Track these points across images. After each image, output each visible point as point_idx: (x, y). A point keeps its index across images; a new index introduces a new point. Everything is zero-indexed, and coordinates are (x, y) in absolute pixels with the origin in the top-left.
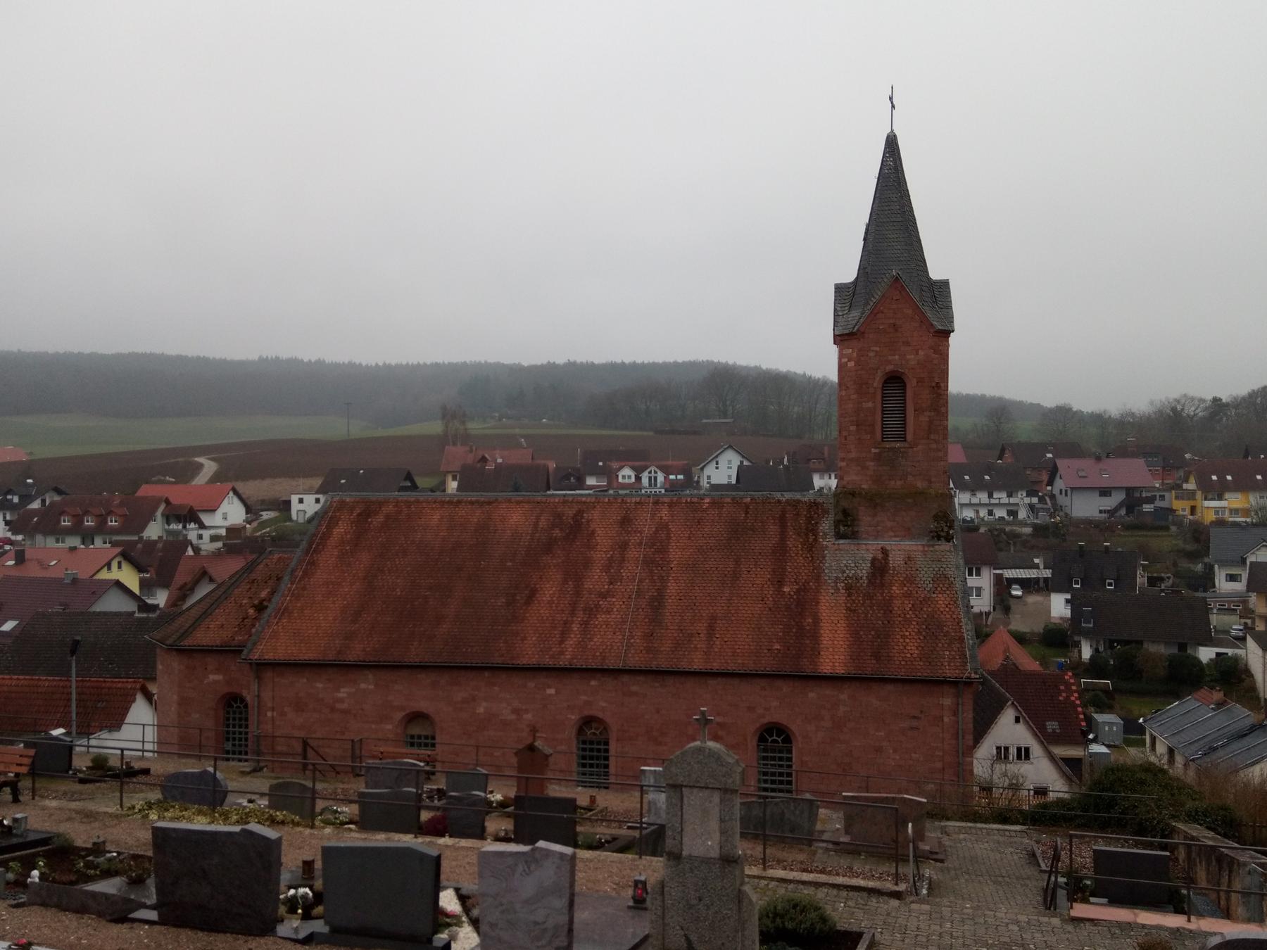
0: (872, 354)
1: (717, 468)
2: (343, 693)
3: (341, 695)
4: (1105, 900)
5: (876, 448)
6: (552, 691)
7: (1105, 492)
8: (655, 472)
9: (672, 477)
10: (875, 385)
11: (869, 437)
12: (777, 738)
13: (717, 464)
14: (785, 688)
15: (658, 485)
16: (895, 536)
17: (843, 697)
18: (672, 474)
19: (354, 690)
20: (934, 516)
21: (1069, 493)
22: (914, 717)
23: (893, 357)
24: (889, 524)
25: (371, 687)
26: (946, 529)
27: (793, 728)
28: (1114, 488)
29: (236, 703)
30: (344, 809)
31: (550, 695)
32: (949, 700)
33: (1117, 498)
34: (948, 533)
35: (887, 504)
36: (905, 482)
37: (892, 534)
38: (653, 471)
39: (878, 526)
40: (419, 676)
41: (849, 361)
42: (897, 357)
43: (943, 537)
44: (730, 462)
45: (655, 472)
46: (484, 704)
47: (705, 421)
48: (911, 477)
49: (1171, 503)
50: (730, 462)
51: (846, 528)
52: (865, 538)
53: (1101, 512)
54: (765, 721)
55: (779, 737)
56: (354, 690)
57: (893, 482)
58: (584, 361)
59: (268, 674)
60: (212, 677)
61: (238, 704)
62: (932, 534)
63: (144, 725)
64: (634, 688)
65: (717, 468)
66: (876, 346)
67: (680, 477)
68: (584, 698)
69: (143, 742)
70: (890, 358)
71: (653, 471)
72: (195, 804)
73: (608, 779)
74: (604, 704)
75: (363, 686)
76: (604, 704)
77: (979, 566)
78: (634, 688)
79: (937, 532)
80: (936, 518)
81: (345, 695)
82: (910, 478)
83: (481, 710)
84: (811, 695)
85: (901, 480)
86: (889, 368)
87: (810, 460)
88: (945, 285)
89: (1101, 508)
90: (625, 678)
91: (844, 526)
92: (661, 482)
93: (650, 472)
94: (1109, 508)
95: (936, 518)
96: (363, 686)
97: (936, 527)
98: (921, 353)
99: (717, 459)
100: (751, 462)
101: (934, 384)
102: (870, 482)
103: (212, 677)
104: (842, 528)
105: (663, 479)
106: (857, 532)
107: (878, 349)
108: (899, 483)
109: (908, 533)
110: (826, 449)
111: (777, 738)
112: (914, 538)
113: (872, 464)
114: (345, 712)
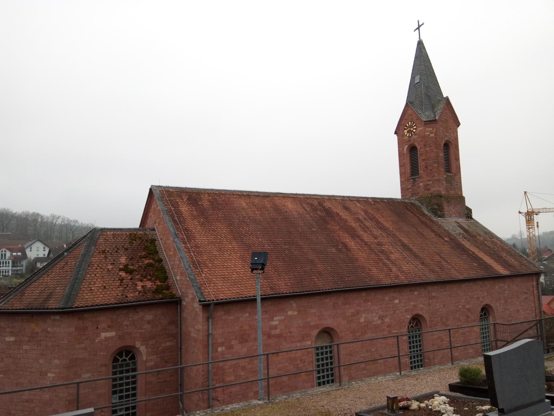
1: (31, 251)
2: (277, 320)
3: (274, 323)
6: (397, 301)
8: (5, 251)
9: (14, 254)
13: (31, 248)
14: (488, 284)
15: (7, 258)
16: (456, 216)
18: (15, 252)
19: (283, 317)
24: (454, 211)
25: (295, 313)
29: (126, 356)
31: (396, 304)
38: (4, 251)
40: (325, 300)
44: (38, 247)
45: (5, 251)
46: (364, 315)
50: (38, 247)
56: (283, 317)
59: (220, 313)
60: (103, 335)
61: (124, 358)
63: (397, 337)
64: (434, 294)
65: (31, 251)
67: (19, 254)
68: (412, 303)
69: (268, 379)
71: (4, 251)
73: (135, 400)
74: (422, 306)
75: (290, 313)
76: (422, 306)
78: (434, 294)
81: (277, 323)
83: (362, 320)
90: (430, 288)
92: (9, 257)
93: (2, 251)
96: (290, 313)
99: (31, 246)
102: (445, 191)
103: (103, 335)
105: (10, 255)
114: (279, 336)
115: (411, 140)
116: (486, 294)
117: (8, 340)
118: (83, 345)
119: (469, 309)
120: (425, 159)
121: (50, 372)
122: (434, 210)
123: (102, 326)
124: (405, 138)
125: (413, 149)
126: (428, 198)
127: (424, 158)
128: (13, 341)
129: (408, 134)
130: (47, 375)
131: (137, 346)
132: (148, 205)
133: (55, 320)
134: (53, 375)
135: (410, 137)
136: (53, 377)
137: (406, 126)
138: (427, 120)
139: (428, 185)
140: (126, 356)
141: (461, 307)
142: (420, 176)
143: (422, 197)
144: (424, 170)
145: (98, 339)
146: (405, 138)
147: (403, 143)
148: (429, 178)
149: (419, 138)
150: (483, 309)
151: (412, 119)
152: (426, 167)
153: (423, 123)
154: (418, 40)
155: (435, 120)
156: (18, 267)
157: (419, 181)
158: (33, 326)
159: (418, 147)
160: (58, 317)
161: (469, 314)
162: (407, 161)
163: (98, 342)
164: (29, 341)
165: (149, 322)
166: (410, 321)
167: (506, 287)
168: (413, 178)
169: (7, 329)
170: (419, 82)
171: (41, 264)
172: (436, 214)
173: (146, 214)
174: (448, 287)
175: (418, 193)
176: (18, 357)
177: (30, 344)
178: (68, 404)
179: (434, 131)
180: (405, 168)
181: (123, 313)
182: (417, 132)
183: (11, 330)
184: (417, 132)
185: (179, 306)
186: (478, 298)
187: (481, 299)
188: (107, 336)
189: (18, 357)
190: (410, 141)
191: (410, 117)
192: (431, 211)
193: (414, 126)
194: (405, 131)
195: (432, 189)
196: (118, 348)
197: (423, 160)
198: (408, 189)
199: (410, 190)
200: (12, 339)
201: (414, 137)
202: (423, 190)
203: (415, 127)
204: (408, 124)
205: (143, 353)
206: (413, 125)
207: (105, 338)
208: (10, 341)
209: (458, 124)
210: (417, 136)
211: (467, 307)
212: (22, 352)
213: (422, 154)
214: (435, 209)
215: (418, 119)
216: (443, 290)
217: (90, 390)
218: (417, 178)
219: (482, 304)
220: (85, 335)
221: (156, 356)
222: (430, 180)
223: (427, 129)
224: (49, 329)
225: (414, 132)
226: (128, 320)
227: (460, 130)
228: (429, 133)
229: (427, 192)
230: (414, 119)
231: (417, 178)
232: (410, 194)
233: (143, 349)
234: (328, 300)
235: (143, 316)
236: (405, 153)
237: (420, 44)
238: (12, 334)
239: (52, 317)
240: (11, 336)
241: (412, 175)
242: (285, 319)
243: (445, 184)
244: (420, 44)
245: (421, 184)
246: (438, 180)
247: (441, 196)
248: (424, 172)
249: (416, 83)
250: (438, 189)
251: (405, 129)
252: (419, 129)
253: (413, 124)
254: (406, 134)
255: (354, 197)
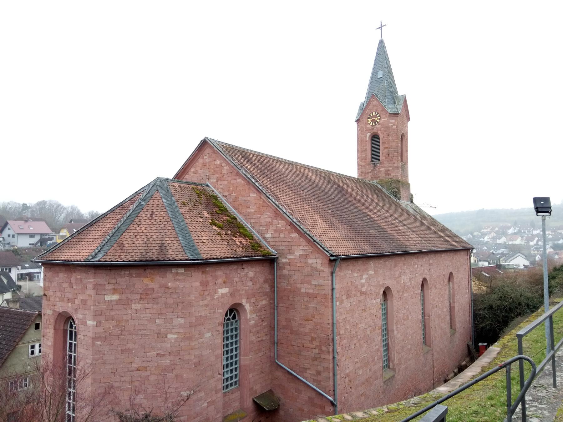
4: (525, 257)
7: (32, 236)
21: (16, 236)
28: (36, 234)
33: (37, 238)
41: (393, 125)
49: (56, 240)
53: (30, 244)
72: (529, 317)
77: (10, 267)
89: (30, 243)
94: (33, 243)
115: (375, 129)
117: (109, 299)
118: (205, 302)
120: (388, 147)
121: (171, 333)
122: (395, 193)
123: (220, 281)
124: (368, 126)
125: (375, 137)
126: (389, 182)
127: (387, 146)
128: (116, 300)
129: (372, 123)
130: (167, 337)
131: (244, 304)
132: (192, 160)
133: (177, 274)
134: (176, 336)
135: (374, 126)
136: (175, 339)
137: (370, 115)
138: (392, 112)
139: (389, 170)
140: (230, 316)
142: (381, 161)
143: (383, 181)
144: (385, 157)
145: (217, 295)
146: (368, 126)
147: (366, 131)
148: (390, 165)
149: (382, 128)
150: (231, 310)
151: (377, 110)
152: (388, 155)
153: (389, 115)
154: (380, 38)
155: (398, 114)
157: (380, 166)
158: (146, 281)
159: (381, 136)
160: (182, 270)
162: (369, 147)
163: (216, 298)
164: (141, 299)
165: (251, 280)
166: (227, 312)
168: (374, 164)
169: (107, 285)
170: (382, 77)
172: (396, 196)
173: (186, 168)
174: (438, 255)
175: (379, 177)
176: (124, 319)
177: (142, 302)
178: (194, 367)
179: (396, 123)
180: (366, 154)
181: (234, 268)
182: (381, 122)
183: (113, 287)
184: (381, 122)
185: (275, 263)
188: (223, 292)
189: (124, 319)
190: (373, 129)
191: (375, 108)
192: (392, 194)
193: (379, 116)
194: (368, 120)
195: (392, 175)
196: (231, 305)
197: (386, 148)
198: (368, 173)
199: (371, 174)
200: (115, 297)
201: (378, 126)
202: (384, 175)
203: (379, 118)
204: (372, 114)
205: (247, 310)
206: (378, 116)
207: (221, 294)
208: (111, 301)
209: (409, 119)
210: (381, 126)
212: (130, 313)
213: (385, 142)
214: (396, 192)
215: (384, 110)
217: (210, 351)
218: (379, 163)
220: (207, 290)
221: (256, 314)
222: (391, 167)
223: (391, 121)
224: (169, 284)
225: (378, 122)
226: (237, 277)
227: (409, 124)
228: (392, 125)
229: (388, 176)
230: (378, 110)
231: (379, 163)
232: (370, 177)
233: (247, 307)
234: (387, 262)
235: (247, 273)
236: (367, 139)
237: (381, 42)
238: (115, 291)
239: (174, 270)
240: (113, 294)
241: (372, 161)
242: (368, 278)
243: (401, 171)
244: (381, 42)
245: (382, 169)
246: (397, 167)
247: (399, 181)
248: (385, 159)
249: (379, 77)
250: (397, 175)
251: (369, 118)
252: (382, 120)
253: (377, 115)
254: (369, 122)
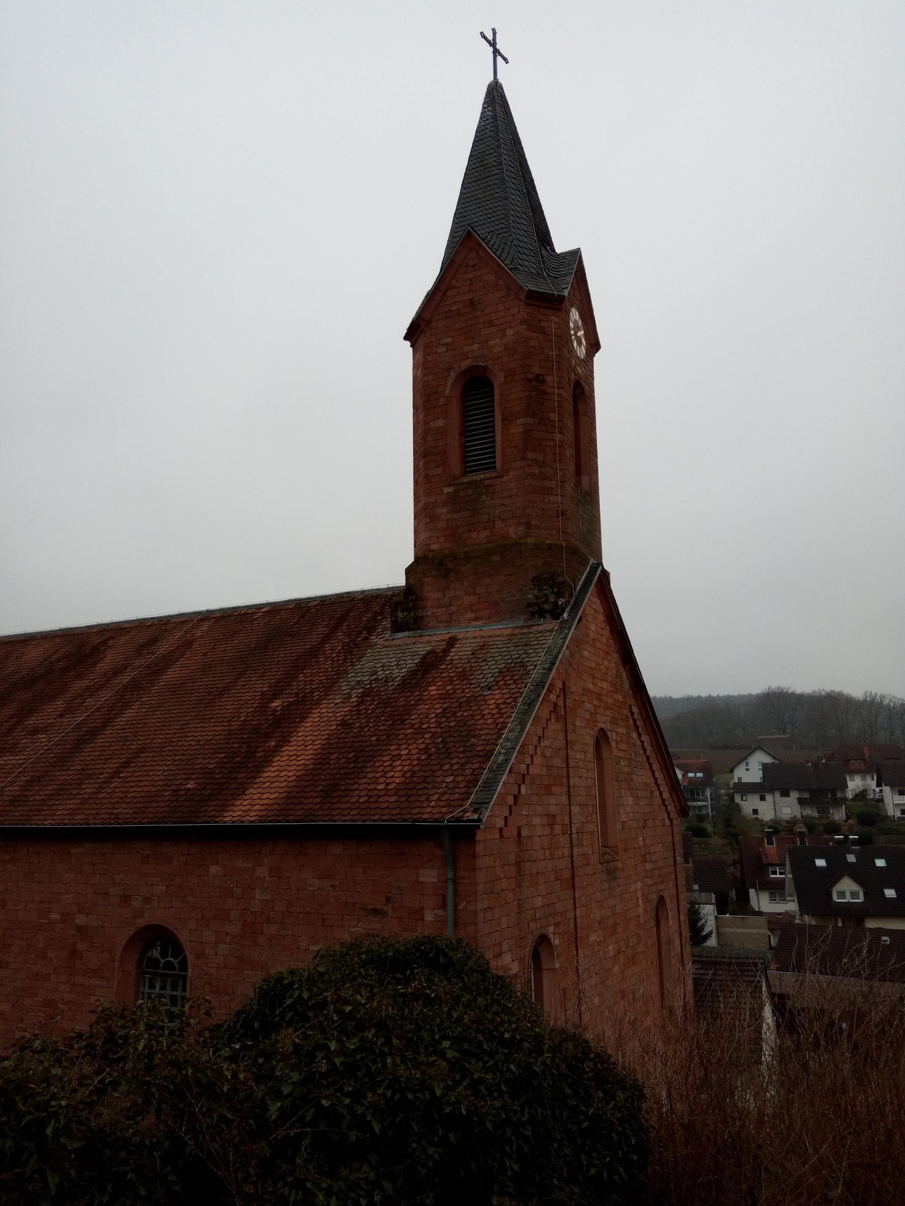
0: (442, 350)
1: (747, 770)
5: (449, 486)
9: (691, 775)
10: (447, 392)
11: (439, 470)
12: (172, 959)
13: (747, 764)
17: (262, 872)
18: (691, 772)
20: (533, 580)
22: (376, 912)
23: (471, 348)
24: (467, 600)
26: (552, 598)
27: (183, 936)
30: (89, 1100)
32: (434, 873)
34: (555, 604)
35: (463, 569)
36: (491, 532)
37: (469, 615)
39: (450, 605)
42: (476, 346)
43: (547, 611)
47: (760, 737)
48: (500, 522)
51: (405, 613)
52: (431, 628)
54: (141, 922)
55: (168, 957)
57: (474, 535)
58: (663, 696)
62: (531, 609)
66: (448, 337)
67: (700, 775)
70: (467, 349)
79: (538, 604)
80: (537, 581)
82: (499, 524)
84: (214, 869)
85: (485, 529)
86: (466, 364)
87: (848, 761)
88: (575, 256)
91: (403, 611)
95: (537, 581)
97: (537, 597)
98: (510, 332)
99: (747, 761)
100: (774, 758)
101: (530, 376)
104: (400, 613)
106: (422, 617)
107: (449, 340)
108: (483, 534)
109: (496, 612)
110: (866, 749)
111: (172, 959)
112: (504, 619)
113: (445, 510)
116: (160, 889)
119: (80, 929)
141: (55, 916)
156: (699, 801)
161: (81, 946)
167: (262, 872)
171: (742, 796)
186: (125, 899)
187: (137, 903)
211: (80, 920)
216: (8, 858)
219: (139, 920)
255: (127, 621)
